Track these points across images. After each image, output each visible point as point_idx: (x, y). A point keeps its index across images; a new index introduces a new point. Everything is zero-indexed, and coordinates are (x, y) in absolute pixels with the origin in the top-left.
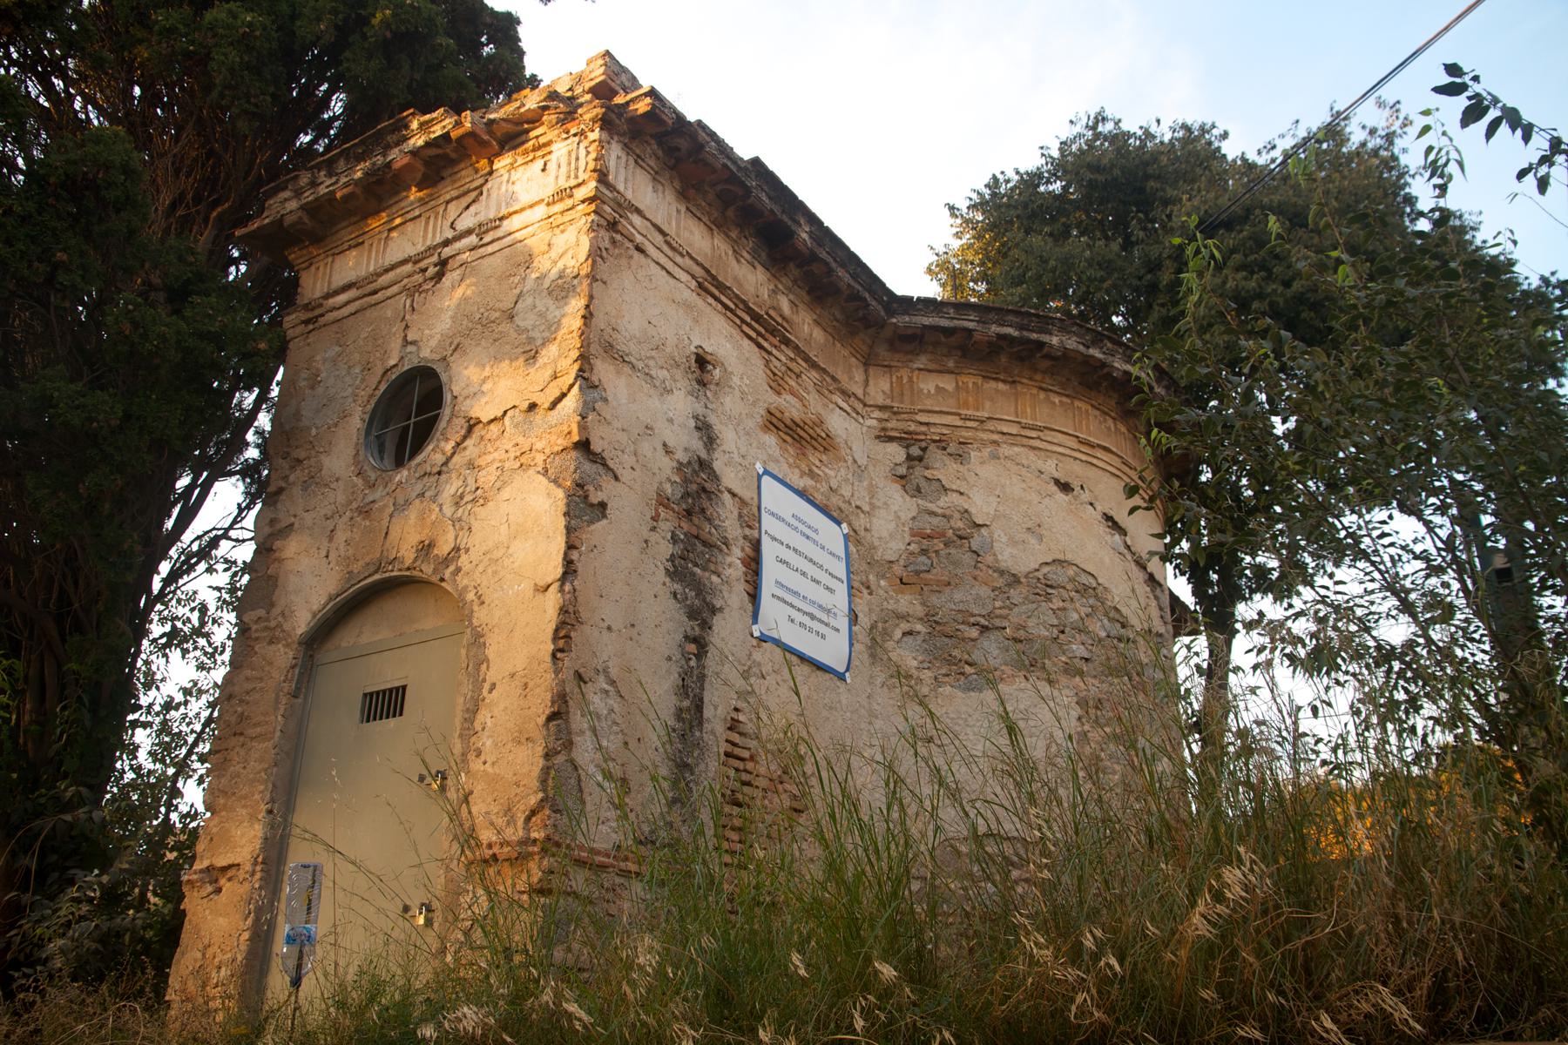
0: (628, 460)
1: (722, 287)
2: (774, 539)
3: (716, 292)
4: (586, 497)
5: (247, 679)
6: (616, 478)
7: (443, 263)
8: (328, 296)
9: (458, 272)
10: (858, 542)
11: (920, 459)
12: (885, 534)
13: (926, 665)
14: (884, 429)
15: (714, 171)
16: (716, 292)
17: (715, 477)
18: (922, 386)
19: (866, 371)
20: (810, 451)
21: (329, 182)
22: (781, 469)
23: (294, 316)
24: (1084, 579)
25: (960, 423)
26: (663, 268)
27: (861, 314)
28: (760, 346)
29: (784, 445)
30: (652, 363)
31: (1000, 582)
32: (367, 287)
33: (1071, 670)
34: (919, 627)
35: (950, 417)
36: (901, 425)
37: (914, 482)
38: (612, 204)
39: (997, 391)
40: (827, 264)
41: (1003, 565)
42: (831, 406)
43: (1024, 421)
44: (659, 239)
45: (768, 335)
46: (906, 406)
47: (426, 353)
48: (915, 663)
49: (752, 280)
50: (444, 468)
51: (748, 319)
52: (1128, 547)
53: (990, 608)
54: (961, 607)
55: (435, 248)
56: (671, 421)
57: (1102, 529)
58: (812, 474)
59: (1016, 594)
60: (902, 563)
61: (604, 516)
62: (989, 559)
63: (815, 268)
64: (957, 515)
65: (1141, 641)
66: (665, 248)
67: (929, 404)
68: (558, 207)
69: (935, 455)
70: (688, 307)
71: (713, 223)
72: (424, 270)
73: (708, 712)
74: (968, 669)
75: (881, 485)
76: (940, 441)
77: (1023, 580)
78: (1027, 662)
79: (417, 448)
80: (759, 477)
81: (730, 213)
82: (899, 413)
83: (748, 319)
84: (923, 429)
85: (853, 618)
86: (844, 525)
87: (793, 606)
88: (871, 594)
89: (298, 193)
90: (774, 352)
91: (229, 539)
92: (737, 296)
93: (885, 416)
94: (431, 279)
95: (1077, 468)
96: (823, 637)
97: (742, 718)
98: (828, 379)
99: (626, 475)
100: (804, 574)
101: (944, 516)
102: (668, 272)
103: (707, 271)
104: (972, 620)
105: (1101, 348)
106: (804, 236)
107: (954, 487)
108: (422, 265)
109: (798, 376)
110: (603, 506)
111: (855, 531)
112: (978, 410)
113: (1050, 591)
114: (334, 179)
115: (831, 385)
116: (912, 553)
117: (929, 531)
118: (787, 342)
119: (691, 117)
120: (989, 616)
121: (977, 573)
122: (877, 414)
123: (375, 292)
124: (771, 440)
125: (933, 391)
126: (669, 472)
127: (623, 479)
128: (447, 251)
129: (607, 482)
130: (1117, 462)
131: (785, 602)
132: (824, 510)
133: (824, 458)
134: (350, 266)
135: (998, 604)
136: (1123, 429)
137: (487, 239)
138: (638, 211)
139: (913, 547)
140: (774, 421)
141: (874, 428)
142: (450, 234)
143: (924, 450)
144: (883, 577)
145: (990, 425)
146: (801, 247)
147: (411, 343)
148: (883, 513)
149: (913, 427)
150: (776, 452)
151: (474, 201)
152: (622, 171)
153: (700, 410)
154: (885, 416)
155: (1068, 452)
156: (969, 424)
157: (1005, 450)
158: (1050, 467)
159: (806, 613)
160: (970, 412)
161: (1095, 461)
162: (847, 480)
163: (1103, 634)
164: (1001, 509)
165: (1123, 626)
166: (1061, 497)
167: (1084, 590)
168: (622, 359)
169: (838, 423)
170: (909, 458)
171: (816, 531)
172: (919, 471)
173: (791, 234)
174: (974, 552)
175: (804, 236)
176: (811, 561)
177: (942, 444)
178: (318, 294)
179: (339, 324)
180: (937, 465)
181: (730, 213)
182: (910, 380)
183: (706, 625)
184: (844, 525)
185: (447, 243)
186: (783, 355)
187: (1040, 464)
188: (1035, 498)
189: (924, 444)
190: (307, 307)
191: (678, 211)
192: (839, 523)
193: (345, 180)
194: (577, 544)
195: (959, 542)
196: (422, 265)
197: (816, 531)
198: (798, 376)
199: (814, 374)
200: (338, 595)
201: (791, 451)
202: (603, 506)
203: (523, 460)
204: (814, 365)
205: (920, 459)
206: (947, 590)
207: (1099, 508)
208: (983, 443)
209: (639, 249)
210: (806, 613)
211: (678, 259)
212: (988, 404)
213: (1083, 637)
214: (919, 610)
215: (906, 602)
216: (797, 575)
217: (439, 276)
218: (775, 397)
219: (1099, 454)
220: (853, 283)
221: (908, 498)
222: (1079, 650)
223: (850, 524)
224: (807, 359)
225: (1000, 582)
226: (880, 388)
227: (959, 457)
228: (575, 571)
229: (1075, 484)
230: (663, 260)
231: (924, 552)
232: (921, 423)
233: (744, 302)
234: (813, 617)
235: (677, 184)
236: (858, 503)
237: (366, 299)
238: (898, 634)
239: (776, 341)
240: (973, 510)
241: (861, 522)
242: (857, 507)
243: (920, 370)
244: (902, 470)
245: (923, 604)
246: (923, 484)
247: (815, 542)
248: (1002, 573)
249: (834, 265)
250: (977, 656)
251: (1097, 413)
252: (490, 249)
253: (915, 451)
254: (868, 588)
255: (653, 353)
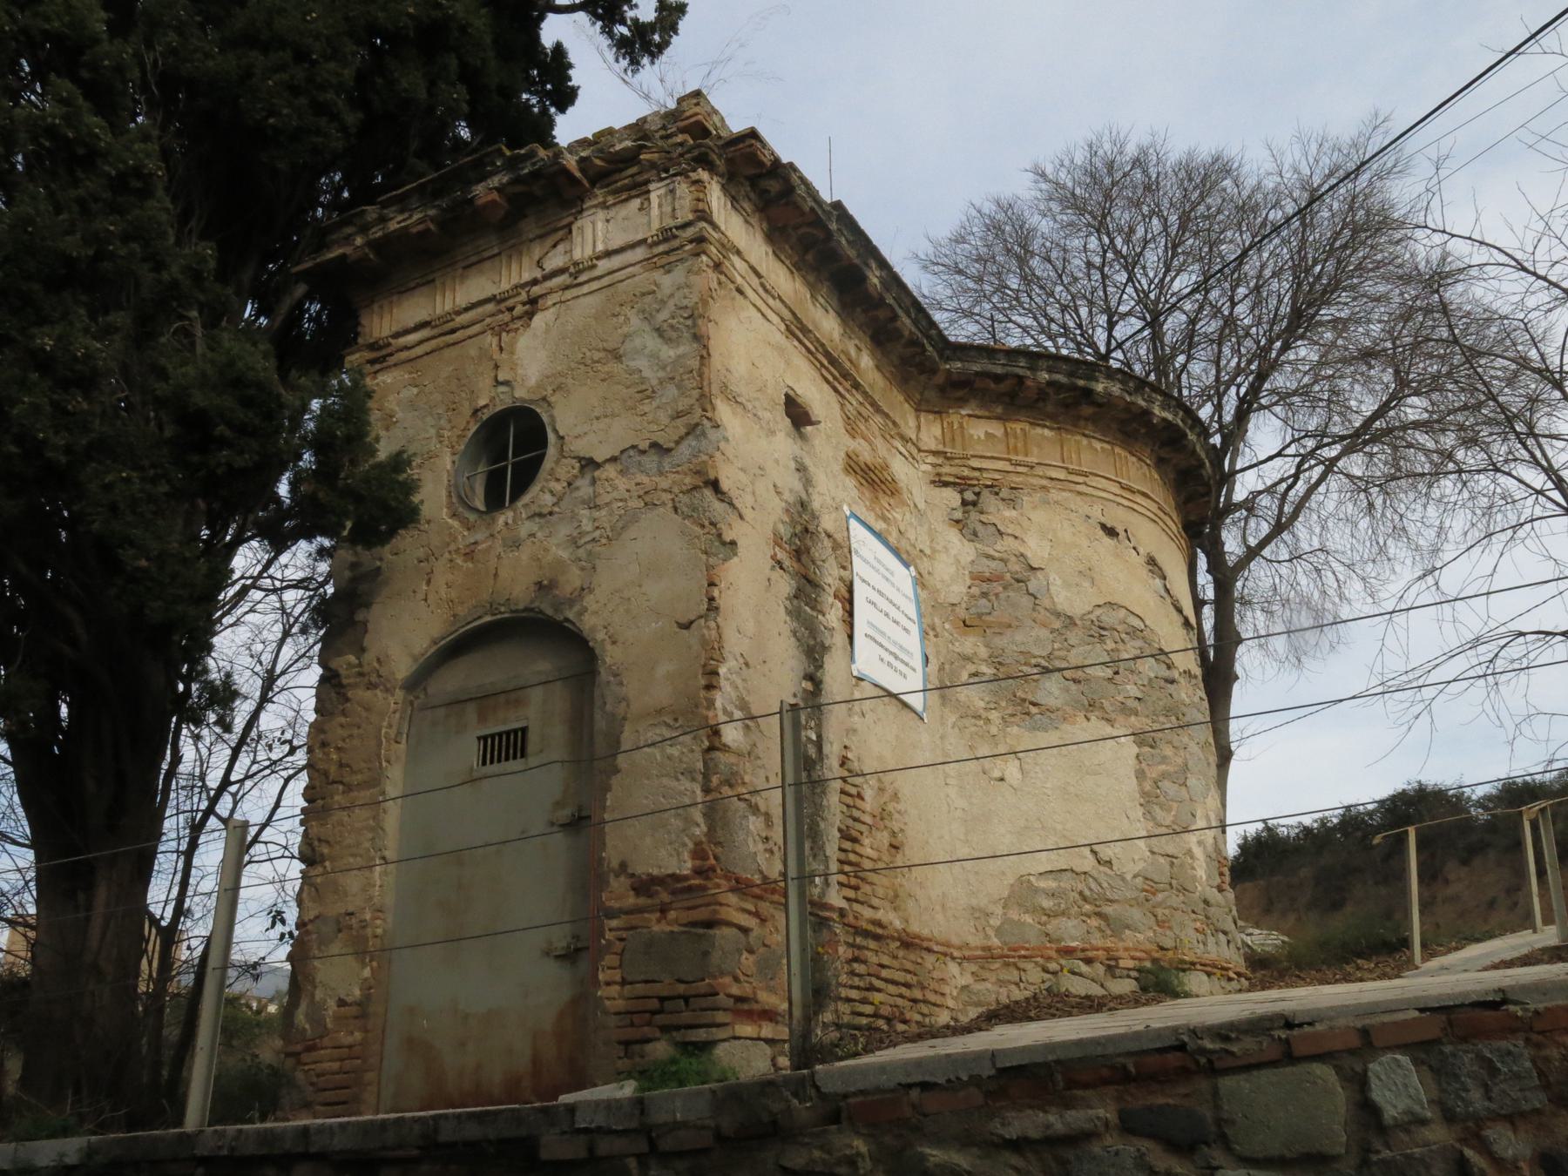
0: (749, 499)
1: (805, 330)
2: (864, 581)
3: (801, 336)
4: (720, 535)
5: (342, 726)
6: (741, 517)
7: (533, 301)
8: (397, 335)
9: (551, 310)
10: (924, 586)
11: (974, 504)
12: (946, 577)
13: (992, 706)
14: (938, 474)
15: (803, 214)
16: (801, 336)
17: (814, 516)
18: (972, 432)
19: (918, 418)
20: (881, 495)
21: (400, 218)
22: (862, 511)
23: (357, 355)
24: (1137, 623)
25: (1011, 468)
26: (759, 310)
27: (917, 359)
28: (836, 390)
29: (861, 488)
30: (757, 404)
31: (1057, 625)
32: (443, 328)
33: (1125, 710)
34: (984, 669)
35: (1002, 463)
36: (954, 470)
37: (971, 526)
38: (717, 245)
39: (1042, 435)
40: (893, 310)
41: (1059, 608)
42: (894, 451)
43: (1071, 467)
44: (755, 281)
45: (841, 380)
46: (958, 451)
47: (520, 393)
48: (982, 704)
49: (828, 324)
50: (556, 509)
51: (826, 363)
52: (1167, 591)
53: (1049, 649)
54: (1022, 648)
55: (523, 286)
56: (777, 461)
57: (1143, 572)
58: (884, 519)
59: (1073, 637)
60: (964, 605)
61: (736, 554)
62: (1046, 602)
63: (882, 314)
64: (1013, 559)
65: (1182, 680)
66: (761, 291)
67: (980, 450)
68: (661, 248)
69: (988, 500)
70: (781, 350)
71: (794, 265)
72: (511, 309)
73: (826, 749)
74: (1034, 710)
75: (940, 530)
76: (992, 486)
77: (1078, 622)
78: (1086, 703)
79: (521, 486)
80: (847, 519)
81: (809, 257)
82: (952, 458)
83: (826, 363)
84: (977, 474)
85: (926, 660)
86: (912, 568)
87: (882, 646)
88: (936, 636)
89: (364, 229)
90: (848, 396)
91: (260, 589)
92: (818, 340)
93: (939, 461)
94: (519, 318)
95: (1121, 513)
96: (905, 677)
97: (850, 755)
98: (890, 424)
99: (747, 513)
100: (887, 615)
101: (1001, 560)
102: (763, 314)
103: (794, 314)
104: (1033, 661)
105: (1143, 395)
106: (875, 281)
107: (1010, 531)
108: (510, 303)
109: (866, 420)
110: (733, 543)
111: (920, 574)
112: (1026, 455)
113: (1103, 633)
114: (406, 215)
115: (893, 431)
116: (973, 596)
117: (987, 575)
118: (857, 386)
119: (785, 160)
120: (1049, 657)
121: (1035, 614)
122: (931, 459)
123: (453, 331)
124: (850, 482)
125: (983, 437)
126: (780, 512)
127: (747, 518)
128: (536, 290)
129: (737, 523)
130: (1153, 507)
131: (876, 641)
132: (896, 552)
133: (892, 502)
134: (413, 309)
135: (1056, 646)
136: (1156, 476)
137: (582, 278)
138: (738, 253)
139: (975, 591)
140: (852, 464)
141: (929, 473)
142: (538, 274)
143: (978, 494)
144: (947, 620)
145: (1039, 471)
146: (871, 289)
147: (502, 383)
148: (943, 557)
149: (966, 472)
150: (855, 493)
151: (562, 240)
152: (722, 211)
153: (798, 452)
154: (939, 461)
155: (1111, 497)
156: (1020, 469)
157: (1055, 495)
158: (1096, 512)
159: (891, 653)
160: (1020, 458)
161: (1135, 506)
162: (911, 524)
163: (1152, 675)
164: (1054, 553)
165: (1169, 667)
166: (1107, 540)
167: (1134, 632)
168: (734, 400)
169: (900, 469)
170: (964, 503)
171: (892, 574)
172: (974, 515)
173: (863, 279)
174: (1032, 595)
175: (875, 281)
176: (891, 602)
177: (994, 488)
178: (386, 332)
179: (411, 364)
180: (992, 509)
181: (809, 257)
182: (961, 426)
183: (820, 666)
184: (912, 568)
185: (535, 282)
186: (855, 399)
187: (1086, 510)
188: (1085, 543)
189: (977, 489)
190: (373, 347)
191: (767, 253)
192: (907, 565)
193: (420, 215)
194: (717, 582)
195: (1016, 585)
196: (510, 303)
197: (892, 574)
198: (866, 420)
199: (878, 419)
200: (444, 638)
201: (867, 494)
202: (733, 543)
203: (647, 499)
204: (878, 410)
205: (974, 504)
206: (1008, 632)
207: (1141, 550)
208: (1034, 488)
209: (740, 291)
210: (891, 653)
211: (771, 301)
212: (1035, 450)
213: (1136, 678)
214: (983, 652)
215: (970, 644)
216: (882, 615)
217: (530, 315)
218: (850, 440)
219: (1139, 499)
220: (913, 329)
221: (966, 542)
222: (1132, 690)
223: (916, 568)
224: (874, 404)
225: (1057, 625)
226: (931, 433)
227: (1011, 502)
228: (717, 608)
229: (1120, 529)
230: (759, 303)
231: (984, 595)
232: (974, 469)
233: (823, 345)
234: (896, 658)
235: (765, 225)
236: (921, 547)
237: (443, 338)
238: (964, 677)
239: (848, 385)
240: (1029, 554)
241: (925, 565)
242: (921, 551)
243: (970, 416)
244: (958, 515)
245: (987, 646)
246: (979, 528)
247: (893, 585)
248: (1058, 615)
249: (900, 312)
250: (1040, 697)
251: (1134, 459)
252: (586, 289)
253: (969, 496)
254: (934, 629)
255: (758, 395)
